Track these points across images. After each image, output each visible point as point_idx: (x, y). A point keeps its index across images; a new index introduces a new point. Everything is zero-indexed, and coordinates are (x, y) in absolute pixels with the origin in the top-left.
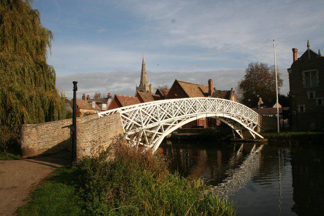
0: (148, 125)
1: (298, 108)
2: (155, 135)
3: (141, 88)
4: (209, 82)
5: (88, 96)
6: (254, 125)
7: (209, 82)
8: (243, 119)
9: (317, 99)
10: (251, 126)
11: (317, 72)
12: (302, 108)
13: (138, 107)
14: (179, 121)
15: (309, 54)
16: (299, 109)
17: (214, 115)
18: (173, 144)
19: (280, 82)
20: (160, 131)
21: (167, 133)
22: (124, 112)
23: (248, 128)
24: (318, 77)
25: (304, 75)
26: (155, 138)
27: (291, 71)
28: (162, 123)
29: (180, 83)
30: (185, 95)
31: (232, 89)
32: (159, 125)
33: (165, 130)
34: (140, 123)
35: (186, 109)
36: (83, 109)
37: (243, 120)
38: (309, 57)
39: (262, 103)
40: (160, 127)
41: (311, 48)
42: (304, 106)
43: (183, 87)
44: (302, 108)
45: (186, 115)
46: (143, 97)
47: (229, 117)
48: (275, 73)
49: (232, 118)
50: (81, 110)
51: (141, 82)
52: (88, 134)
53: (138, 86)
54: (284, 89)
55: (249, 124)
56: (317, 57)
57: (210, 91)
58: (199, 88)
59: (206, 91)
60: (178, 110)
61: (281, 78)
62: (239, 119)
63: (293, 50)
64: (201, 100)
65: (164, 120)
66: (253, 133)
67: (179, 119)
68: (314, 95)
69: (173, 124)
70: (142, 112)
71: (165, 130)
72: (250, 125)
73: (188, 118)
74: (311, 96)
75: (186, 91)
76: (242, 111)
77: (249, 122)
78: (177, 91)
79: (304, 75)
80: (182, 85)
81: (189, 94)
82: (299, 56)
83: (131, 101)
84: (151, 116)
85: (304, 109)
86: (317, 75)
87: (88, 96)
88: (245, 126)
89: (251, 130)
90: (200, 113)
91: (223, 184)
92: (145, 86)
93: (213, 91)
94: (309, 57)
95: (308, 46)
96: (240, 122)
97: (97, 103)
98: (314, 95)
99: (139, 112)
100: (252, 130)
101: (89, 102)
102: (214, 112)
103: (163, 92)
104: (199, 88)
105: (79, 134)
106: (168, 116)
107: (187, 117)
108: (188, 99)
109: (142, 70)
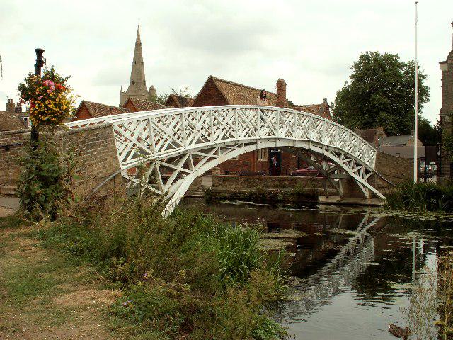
0: (129, 160)
6: (367, 172)
10: (362, 172)
19: (424, 92)
20: (186, 166)
23: (354, 175)
26: (176, 180)
27: (446, 68)
32: (185, 155)
33: (195, 165)
37: (346, 160)
40: (186, 157)
48: (413, 74)
54: (431, 112)
61: (425, 83)
66: (364, 186)
69: (211, 155)
71: (195, 165)
72: (359, 171)
76: (333, 136)
84: (137, 143)
88: (351, 171)
89: (361, 180)
91: (281, 134)
100: (363, 181)
106: (174, 142)
107: (239, 143)
108: (224, 107)
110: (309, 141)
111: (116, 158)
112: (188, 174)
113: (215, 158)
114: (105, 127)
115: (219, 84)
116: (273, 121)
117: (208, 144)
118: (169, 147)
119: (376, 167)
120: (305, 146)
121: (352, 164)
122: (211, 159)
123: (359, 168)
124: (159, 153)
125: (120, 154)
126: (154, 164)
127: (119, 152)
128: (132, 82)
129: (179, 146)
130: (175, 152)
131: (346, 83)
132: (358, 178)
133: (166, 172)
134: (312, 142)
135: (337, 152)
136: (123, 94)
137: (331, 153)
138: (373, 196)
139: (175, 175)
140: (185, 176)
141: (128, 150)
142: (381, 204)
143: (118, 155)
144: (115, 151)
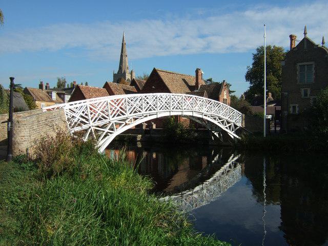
0: (96, 122)
1: (290, 107)
2: (104, 134)
3: (119, 77)
4: (197, 71)
5: (48, 84)
7: (197, 71)
8: (220, 119)
9: (312, 98)
11: (314, 66)
12: (294, 107)
13: (109, 99)
14: (136, 119)
15: (306, 42)
16: (291, 109)
17: (167, 114)
18: (83, 143)
21: (120, 131)
22: (91, 103)
24: (314, 72)
25: (298, 68)
26: (105, 136)
28: (114, 120)
29: (160, 73)
30: (165, 89)
31: (224, 81)
34: (87, 120)
35: (184, 104)
36: (39, 100)
37: (220, 121)
38: (305, 46)
39: (272, 99)
41: (309, 36)
42: (297, 105)
43: (162, 77)
44: (294, 107)
45: (143, 112)
46: (113, 89)
47: (201, 116)
49: (205, 118)
50: (37, 102)
51: (120, 68)
52: (25, 129)
53: (116, 72)
55: (228, 126)
56: (315, 47)
57: (197, 83)
58: (184, 80)
59: (193, 84)
60: (116, 106)
62: (215, 119)
63: (291, 37)
64: (176, 97)
65: (116, 118)
67: (135, 117)
68: (309, 93)
70: (110, 104)
72: (230, 127)
73: (146, 116)
74: (306, 94)
75: (166, 84)
77: (228, 123)
78: (155, 83)
79: (298, 68)
80: (161, 74)
81: (169, 87)
82: (296, 43)
83: (96, 93)
85: (297, 109)
86: (313, 68)
87: (48, 84)
92: (125, 73)
93: (202, 83)
94: (305, 46)
95: (305, 34)
96: (216, 122)
97: (59, 94)
98: (309, 93)
99: (125, 101)
101: (48, 93)
102: (167, 110)
103: (140, 82)
104: (184, 80)
105: (16, 129)
108: (171, 94)
109: (122, 56)
122: (126, 124)
129: (123, 114)
136: (115, 75)
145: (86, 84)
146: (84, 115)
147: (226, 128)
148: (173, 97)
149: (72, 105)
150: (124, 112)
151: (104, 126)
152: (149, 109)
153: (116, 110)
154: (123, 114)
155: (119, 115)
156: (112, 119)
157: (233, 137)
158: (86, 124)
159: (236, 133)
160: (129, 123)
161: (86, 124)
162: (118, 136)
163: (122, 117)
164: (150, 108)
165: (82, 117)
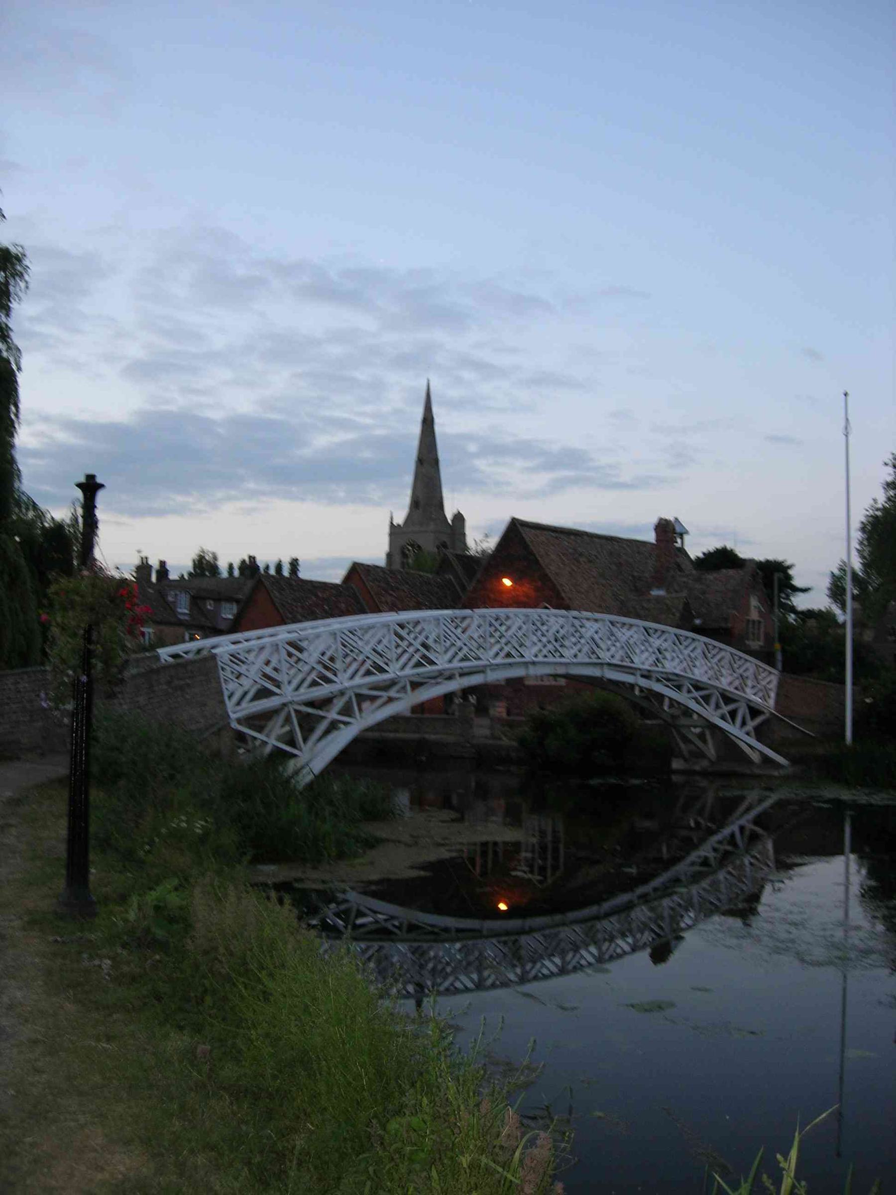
0: (244, 704)
6: (754, 712)
14: (415, 685)
20: (347, 711)
26: (327, 732)
34: (278, 685)
53: (399, 519)
55: (726, 709)
62: (679, 687)
69: (392, 693)
72: (733, 714)
73: (450, 678)
77: (728, 699)
90: (499, 660)
106: (424, 657)
107: (447, 674)
110: (602, 664)
111: (222, 702)
112: (346, 724)
113: (397, 699)
114: (205, 659)
115: (528, 535)
116: (520, 634)
117: (385, 676)
118: (419, 664)
119: (777, 702)
120: (596, 672)
121: (713, 701)
122: (390, 700)
123: (731, 707)
124: (296, 693)
125: (230, 697)
126: (286, 709)
127: (226, 694)
128: (415, 504)
129: (432, 663)
130: (324, 690)
131: (875, 500)
132: (733, 729)
133: (308, 724)
134: (609, 664)
135: (675, 681)
136: (395, 531)
137: (658, 680)
138: (766, 760)
139: (323, 726)
140: (342, 726)
141: (300, 677)
142: (776, 773)
143: (226, 698)
144: (221, 693)
145: (294, 564)
146: (268, 670)
147: (723, 718)
148: (577, 623)
149: (246, 641)
150: (329, 675)
151: (325, 703)
152: (362, 671)
153: (411, 650)
154: (328, 681)
155: (368, 673)
156: (347, 684)
157: (755, 757)
158: (275, 694)
159: (760, 733)
160: (398, 695)
161: (275, 694)
162: (356, 741)
163: (379, 677)
164: (507, 649)
165: (265, 676)
